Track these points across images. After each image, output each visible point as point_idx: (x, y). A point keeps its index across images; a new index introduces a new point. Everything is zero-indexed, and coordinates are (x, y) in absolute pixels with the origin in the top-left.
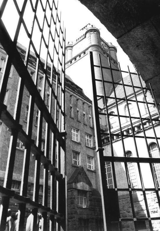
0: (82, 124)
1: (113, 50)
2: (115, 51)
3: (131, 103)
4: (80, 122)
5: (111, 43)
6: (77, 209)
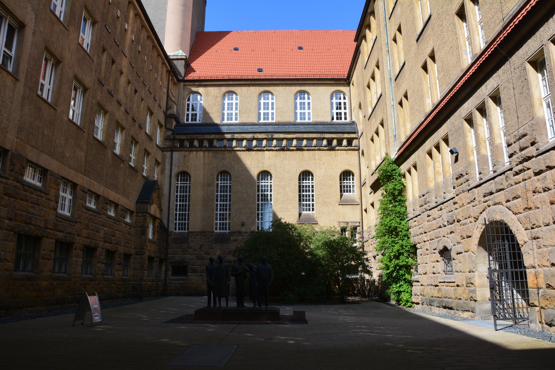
0: (157, 105)
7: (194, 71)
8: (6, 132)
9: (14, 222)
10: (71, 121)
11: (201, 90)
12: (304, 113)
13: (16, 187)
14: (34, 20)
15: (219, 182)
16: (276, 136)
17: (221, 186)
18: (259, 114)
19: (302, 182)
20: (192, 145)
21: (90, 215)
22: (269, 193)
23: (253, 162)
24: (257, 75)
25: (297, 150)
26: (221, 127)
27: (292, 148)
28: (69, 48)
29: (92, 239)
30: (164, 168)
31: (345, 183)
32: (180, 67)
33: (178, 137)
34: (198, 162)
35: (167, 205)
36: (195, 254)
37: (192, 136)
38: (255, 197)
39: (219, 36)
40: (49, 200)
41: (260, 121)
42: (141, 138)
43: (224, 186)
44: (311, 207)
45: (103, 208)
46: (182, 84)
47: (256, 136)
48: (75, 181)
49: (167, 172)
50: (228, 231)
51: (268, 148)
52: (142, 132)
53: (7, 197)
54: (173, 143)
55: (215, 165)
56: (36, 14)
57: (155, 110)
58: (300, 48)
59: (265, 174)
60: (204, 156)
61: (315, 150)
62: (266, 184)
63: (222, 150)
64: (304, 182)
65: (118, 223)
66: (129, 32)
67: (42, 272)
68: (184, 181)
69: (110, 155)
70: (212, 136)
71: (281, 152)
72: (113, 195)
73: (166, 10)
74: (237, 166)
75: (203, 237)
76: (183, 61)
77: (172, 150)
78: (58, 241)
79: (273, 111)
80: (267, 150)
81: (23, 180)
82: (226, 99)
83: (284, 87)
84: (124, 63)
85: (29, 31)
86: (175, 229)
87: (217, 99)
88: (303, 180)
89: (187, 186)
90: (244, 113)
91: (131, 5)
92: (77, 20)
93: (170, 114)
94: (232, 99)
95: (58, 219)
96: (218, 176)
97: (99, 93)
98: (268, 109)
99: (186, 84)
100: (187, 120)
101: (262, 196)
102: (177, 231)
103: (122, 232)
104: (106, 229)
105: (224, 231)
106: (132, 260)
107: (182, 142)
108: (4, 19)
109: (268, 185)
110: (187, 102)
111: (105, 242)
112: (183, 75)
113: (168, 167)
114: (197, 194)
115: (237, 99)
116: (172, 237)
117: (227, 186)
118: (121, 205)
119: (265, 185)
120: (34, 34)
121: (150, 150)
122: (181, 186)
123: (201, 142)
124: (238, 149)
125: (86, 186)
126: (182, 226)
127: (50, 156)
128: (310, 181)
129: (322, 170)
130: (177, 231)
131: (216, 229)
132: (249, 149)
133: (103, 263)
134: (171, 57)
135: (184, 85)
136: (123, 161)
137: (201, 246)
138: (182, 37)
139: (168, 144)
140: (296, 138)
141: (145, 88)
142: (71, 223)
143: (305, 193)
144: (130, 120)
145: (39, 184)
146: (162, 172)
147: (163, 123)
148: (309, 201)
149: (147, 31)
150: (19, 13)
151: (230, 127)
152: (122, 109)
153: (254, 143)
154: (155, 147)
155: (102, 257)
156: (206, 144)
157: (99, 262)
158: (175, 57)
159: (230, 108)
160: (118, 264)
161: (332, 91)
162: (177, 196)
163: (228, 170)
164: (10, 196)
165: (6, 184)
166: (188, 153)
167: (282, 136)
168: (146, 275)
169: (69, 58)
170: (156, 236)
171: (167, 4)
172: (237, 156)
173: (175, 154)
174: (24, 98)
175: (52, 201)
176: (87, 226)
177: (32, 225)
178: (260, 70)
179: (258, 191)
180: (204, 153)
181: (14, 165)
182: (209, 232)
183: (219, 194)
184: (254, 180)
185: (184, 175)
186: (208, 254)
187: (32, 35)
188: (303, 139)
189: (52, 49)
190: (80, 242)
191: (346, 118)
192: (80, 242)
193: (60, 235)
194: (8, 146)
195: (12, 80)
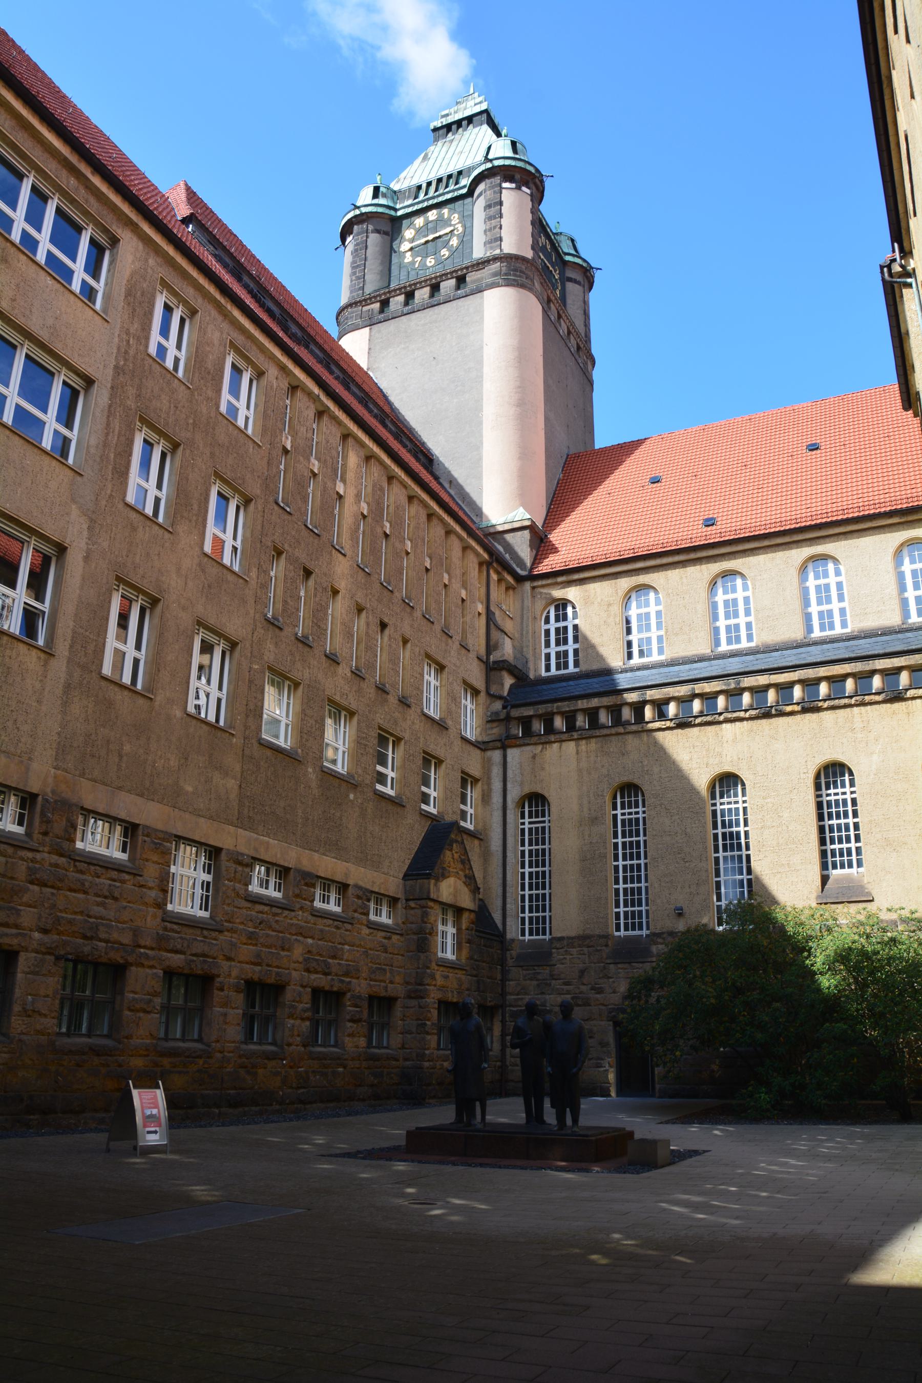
0: (456, 646)
1: (578, 283)
2: (586, 287)
3: (183, 196)
4: (451, 637)
5: (573, 241)
6: (436, 968)
7: (555, 550)
8: (30, 759)
9: (56, 937)
10: (196, 718)
11: (572, 593)
12: (830, 612)
13: (56, 865)
14: (85, 533)
15: (619, 811)
16: (748, 682)
17: (623, 821)
18: (716, 630)
19: (824, 792)
20: (550, 729)
21: (261, 912)
22: (742, 829)
23: (697, 754)
24: (699, 535)
25: (805, 711)
26: (617, 676)
27: (789, 709)
28: (179, 570)
29: (268, 965)
30: (490, 790)
31: (833, 794)
32: (522, 545)
33: (515, 713)
34: (565, 768)
35: (501, 876)
36: (568, 993)
37: (549, 707)
38: (704, 841)
39: (622, 451)
40: (142, 886)
41: (910, 621)
42: (409, 725)
43: (630, 820)
44: (854, 857)
45: (297, 896)
46: (528, 585)
47: (699, 688)
48: (212, 842)
49: (497, 799)
50: (645, 932)
51: (729, 715)
52: (412, 714)
53: (36, 888)
54: (508, 729)
55: (605, 771)
56: (91, 520)
57: (452, 657)
58: (814, 448)
59: (727, 782)
60: (577, 753)
61: (850, 706)
62: (733, 806)
63: (618, 734)
64: (832, 791)
65: (349, 927)
66: (349, 500)
67: (129, 1037)
68: (537, 817)
69: (313, 776)
70: (595, 702)
71: (764, 722)
72: (327, 865)
73: (481, 423)
74: (656, 769)
75: (586, 950)
76: (527, 533)
77: (504, 743)
78: (170, 974)
79: (842, 605)
80: (727, 721)
81: (75, 850)
82: (811, 575)
83: (770, 555)
84: (341, 571)
85: (75, 558)
86: (523, 934)
87: (611, 608)
88: (828, 788)
89: (543, 828)
90: (677, 634)
91: (350, 440)
92: (195, 507)
93: (494, 662)
94: (826, 575)
95: (168, 924)
96: (615, 798)
97: (270, 646)
98: (829, 601)
99: (536, 584)
100: (548, 669)
101: (724, 839)
102: (527, 937)
103: (359, 946)
104: (310, 941)
105: (637, 933)
106: (398, 1011)
107: (526, 723)
108: (26, 544)
109: (737, 809)
110: (544, 627)
111: (308, 970)
112: (529, 565)
113: (497, 785)
114: (566, 845)
115: (658, 602)
116: (514, 953)
117: (637, 820)
118: (357, 886)
119: (730, 810)
120: (87, 558)
121: (440, 752)
122: (530, 830)
123: (570, 718)
124: (657, 725)
125: (246, 851)
126: (538, 925)
127: (141, 795)
128: (847, 789)
129: (875, 757)
130: (527, 937)
131: (618, 929)
132: (683, 724)
133: (302, 1019)
134: (500, 528)
135: (533, 588)
136: (355, 786)
137: (582, 972)
138: (523, 476)
139: (496, 731)
140: (800, 681)
141: (411, 614)
142: (205, 932)
143: (834, 822)
144: (371, 692)
145: (124, 857)
146: (486, 798)
147: (480, 684)
148: (848, 840)
149: (405, 486)
150: (50, 530)
151: (638, 673)
152: (343, 670)
153: (697, 705)
154: (458, 742)
155: (301, 1006)
156: (581, 721)
157: (291, 1016)
158: (507, 527)
159: (731, 612)
160: (352, 1021)
161: (897, 543)
162: (523, 852)
163: (636, 781)
164: (43, 884)
165: (33, 860)
166: (540, 747)
167: (763, 680)
168: (434, 1044)
169: (178, 587)
170: (465, 953)
171: (481, 410)
172: (656, 743)
173: (513, 754)
174: (68, 687)
175: (150, 888)
176: (252, 937)
177: (100, 940)
178: (710, 523)
179: (715, 827)
180: (577, 746)
181: (48, 822)
182: (600, 937)
183: (620, 840)
184: (701, 798)
185: (536, 801)
186: (600, 991)
187: (82, 563)
188: (818, 681)
189: (134, 579)
190: (231, 973)
191: (844, 624)
192: (231, 973)
193: (176, 960)
194: (35, 790)
195: (39, 658)
